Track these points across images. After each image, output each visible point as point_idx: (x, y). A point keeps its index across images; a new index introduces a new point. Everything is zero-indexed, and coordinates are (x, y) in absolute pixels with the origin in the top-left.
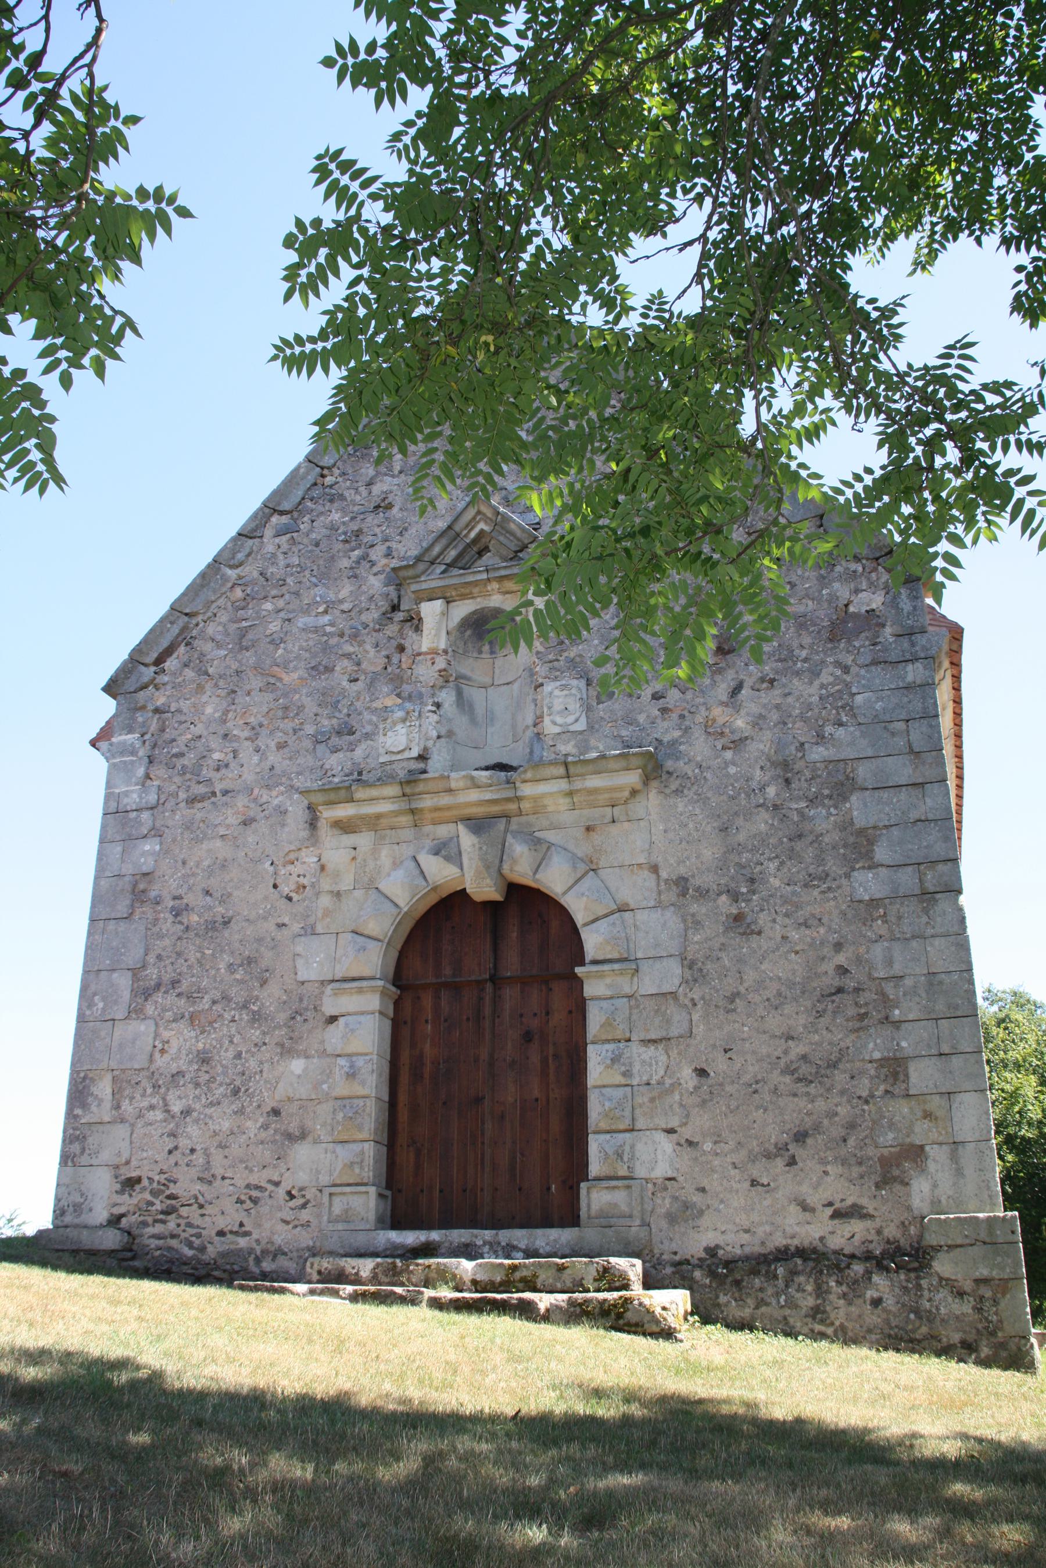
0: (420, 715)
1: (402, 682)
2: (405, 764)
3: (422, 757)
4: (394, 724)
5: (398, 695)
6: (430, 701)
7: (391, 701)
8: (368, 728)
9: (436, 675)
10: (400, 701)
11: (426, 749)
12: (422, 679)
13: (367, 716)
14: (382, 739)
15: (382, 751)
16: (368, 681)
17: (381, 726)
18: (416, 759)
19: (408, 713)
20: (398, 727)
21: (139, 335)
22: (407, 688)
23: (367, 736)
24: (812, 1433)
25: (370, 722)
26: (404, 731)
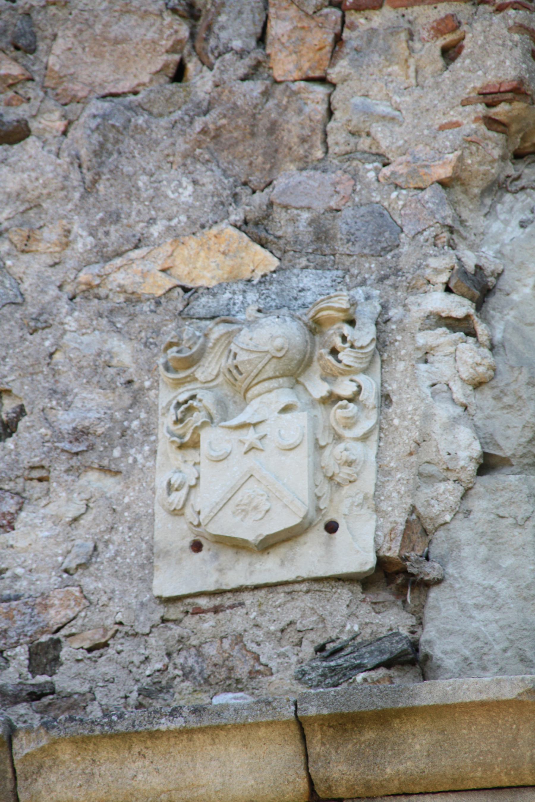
0: (381, 343)
1: (273, 157)
2: (299, 609)
3: (395, 577)
4: (240, 384)
5: (257, 229)
6: (440, 265)
7: (214, 258)
8: (90, 405)
9: (469, 119)
10: (263, 260)
11: (418, 528)
12: (385, 138)
13: (79, 336)
14: (168, 466)
15: (172, 534)
16: (82, 140)
17: (166, 397)
18: (364, 582)
19: (315, 327)
20: (266, 403)
21: (246, 453)
22: (302, 191)
23: (83, 446)
24: (409, 675)
25: (99, 369)
26: (296, 427)
